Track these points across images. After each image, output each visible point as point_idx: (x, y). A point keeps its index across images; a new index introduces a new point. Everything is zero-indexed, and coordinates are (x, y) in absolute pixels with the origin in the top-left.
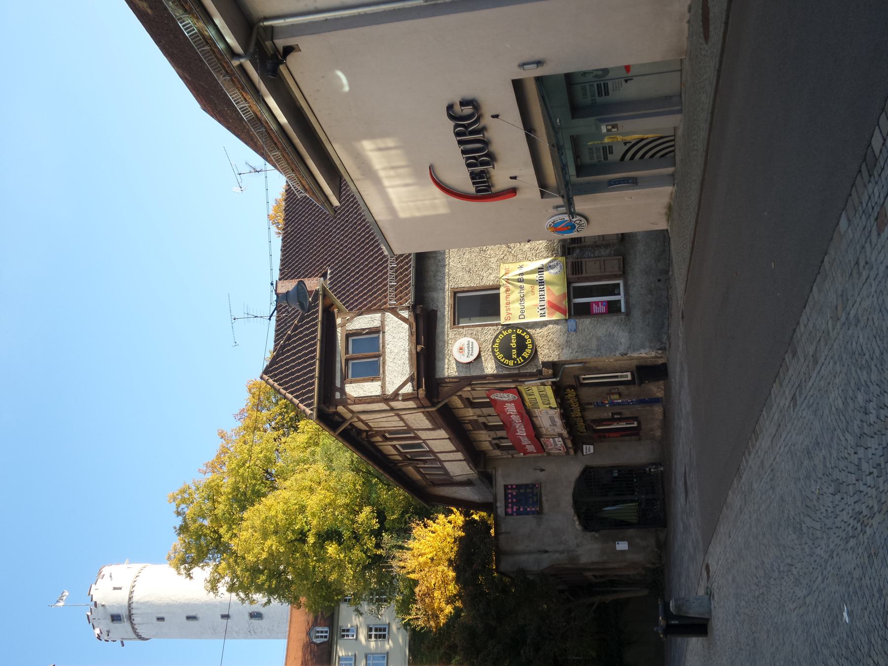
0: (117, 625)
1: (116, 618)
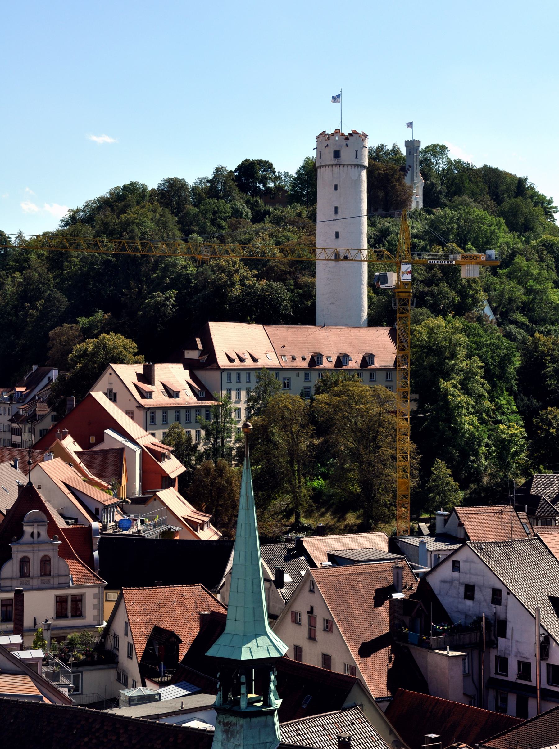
0: (332, 155)
1: (337, 154)
